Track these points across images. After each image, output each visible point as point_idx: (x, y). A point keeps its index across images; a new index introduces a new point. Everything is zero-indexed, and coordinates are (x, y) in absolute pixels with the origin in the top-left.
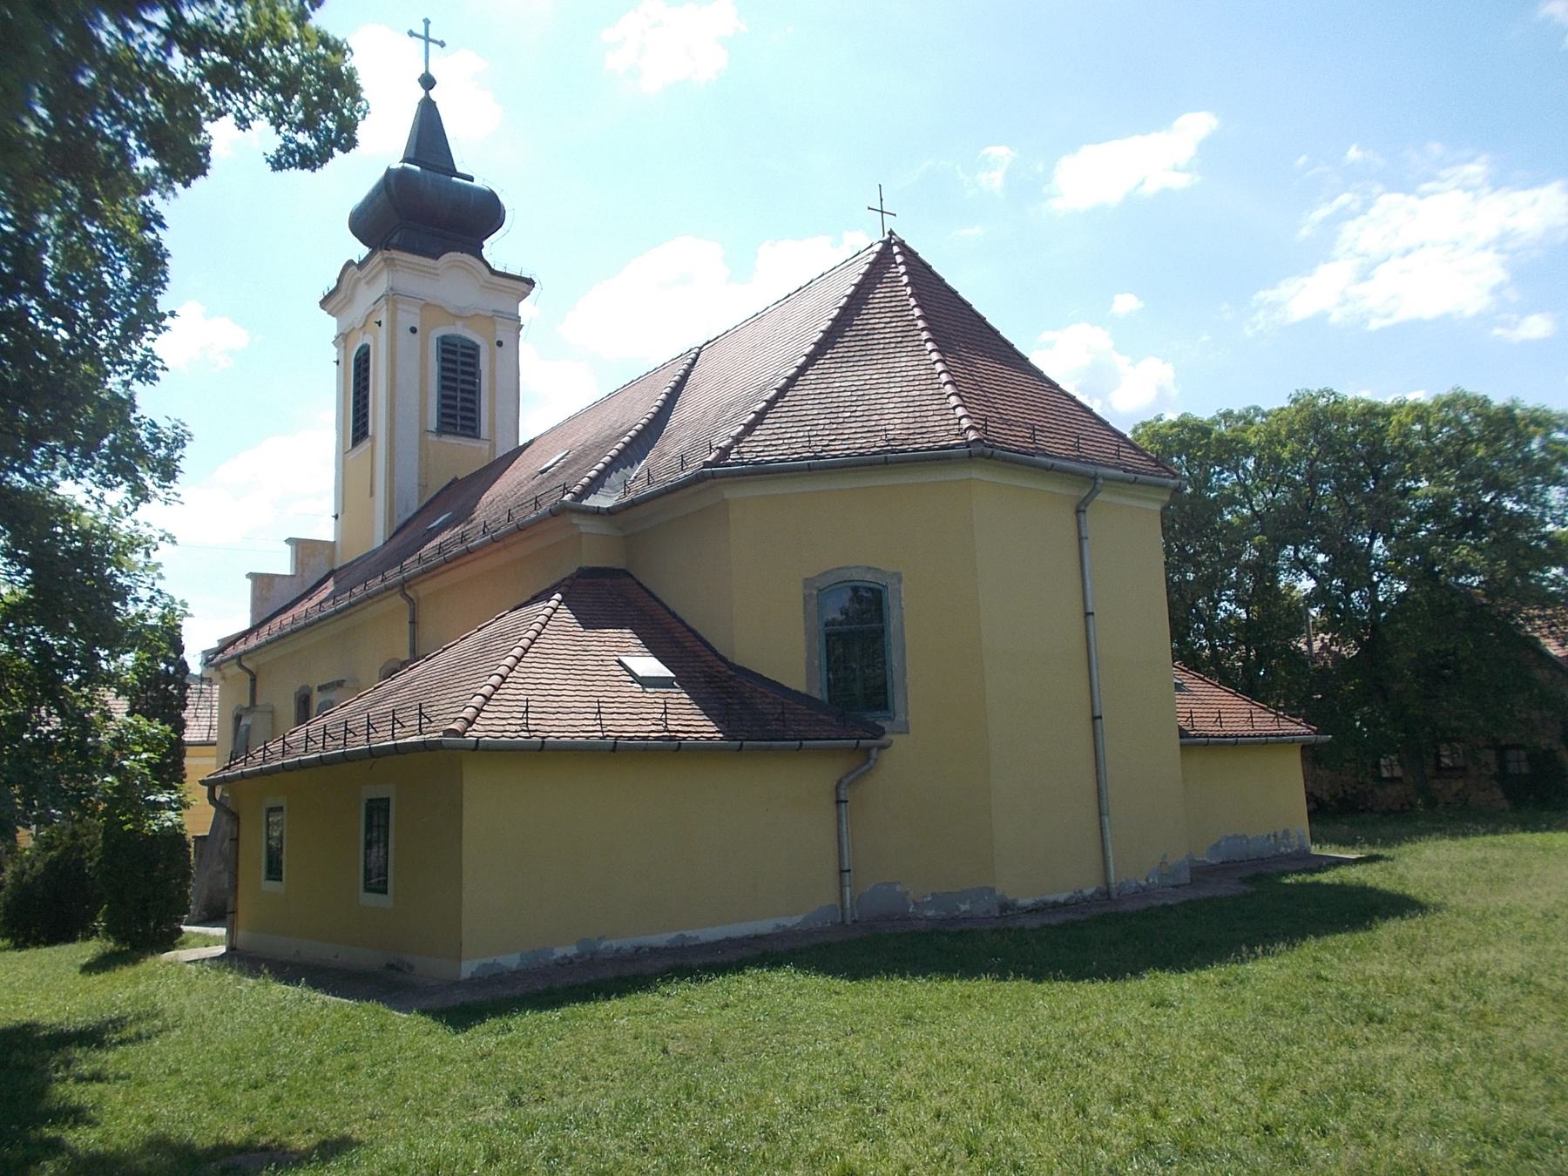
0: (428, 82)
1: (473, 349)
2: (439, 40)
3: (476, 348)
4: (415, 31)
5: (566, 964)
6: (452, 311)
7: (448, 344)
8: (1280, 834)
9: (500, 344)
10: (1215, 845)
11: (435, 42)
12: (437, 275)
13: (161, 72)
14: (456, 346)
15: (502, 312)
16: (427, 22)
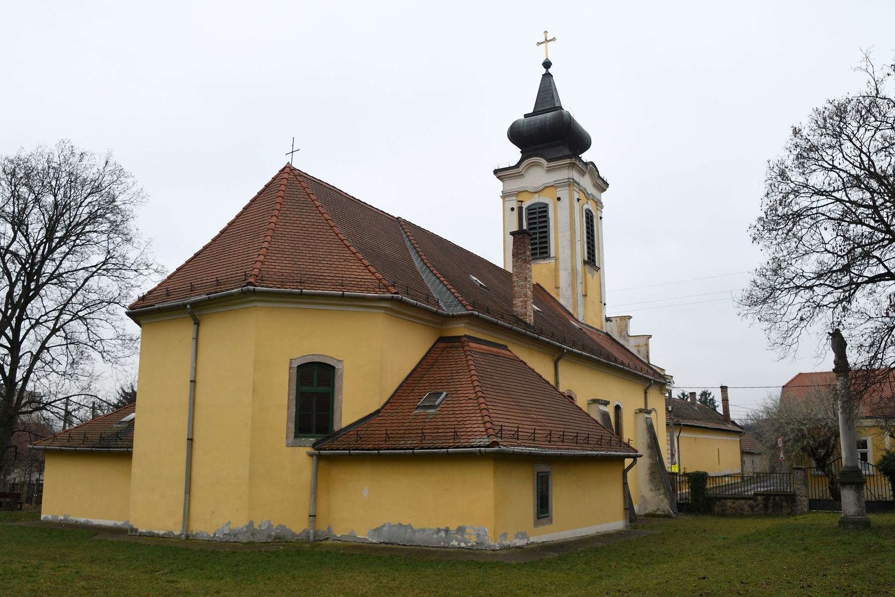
0: (547, 64)
1: (545, 207)
6: (532, 191)
8: (453, 528)
10: (378, 529)
11: (546, 36)
12: (522, 175)
16: (554, 39)
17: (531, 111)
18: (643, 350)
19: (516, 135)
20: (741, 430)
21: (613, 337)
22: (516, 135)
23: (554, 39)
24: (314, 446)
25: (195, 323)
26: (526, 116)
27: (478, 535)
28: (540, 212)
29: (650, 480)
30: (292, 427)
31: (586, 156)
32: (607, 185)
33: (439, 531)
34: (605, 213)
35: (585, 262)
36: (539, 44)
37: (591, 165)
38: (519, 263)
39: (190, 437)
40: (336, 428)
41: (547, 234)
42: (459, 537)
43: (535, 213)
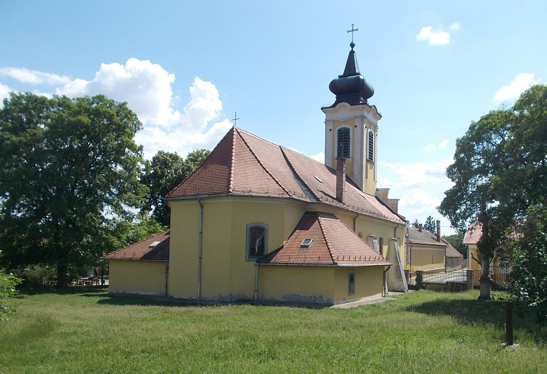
2: (352, 26)
3: (339, 130)
4: (354, 26)
5: (120, 294)
7: (341, 131)
8: (318, 296)
9: (356, 126)
10: (284, 296)
13: (14, 155)
14: (343, 131)
15: (356, 116)
16: (357, 30)
17: (342, 74)
18: (394, 206)
19: (334, 87)
20: (447, 245)
21: (380, 199)
22: (334, 87)
23: (357, 30)
24: (257, 261)
25: (201, 207)
26: (340, 77)
27: (328, 299)
28: (345, 133)
29: (396, 274)
30: (248, 253)
31: (371, 101)
32: (381, 116)
33: (311, 297)
34: (379, 132)
35: (367, 160)
36: (348, 32)
37: (373, 107)
38: (340, 174)
39: (200, 257)
40: (266, 254)
41: (349, 142)
42: (320, 299)
43: (342, 133)
